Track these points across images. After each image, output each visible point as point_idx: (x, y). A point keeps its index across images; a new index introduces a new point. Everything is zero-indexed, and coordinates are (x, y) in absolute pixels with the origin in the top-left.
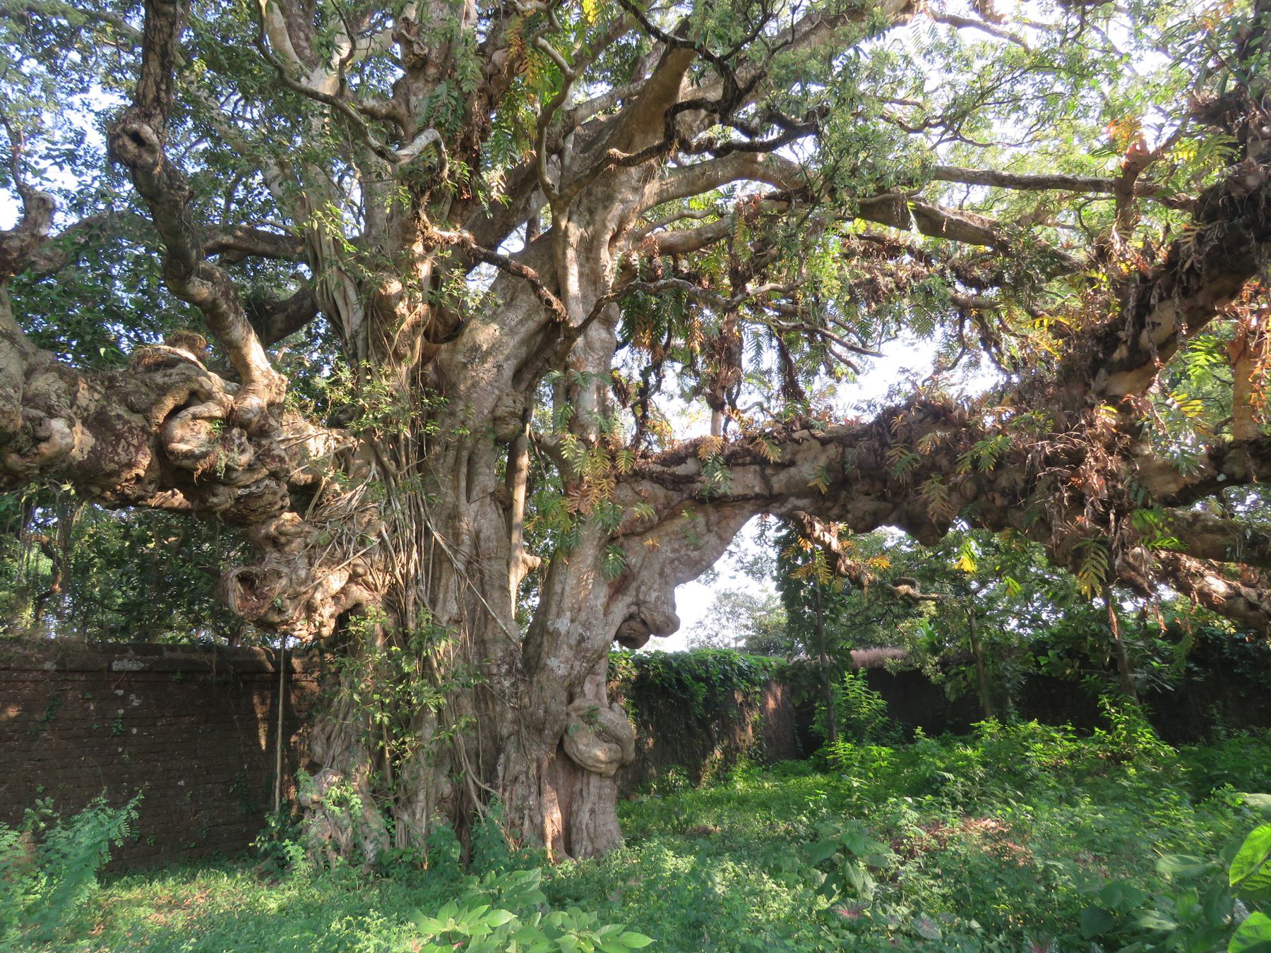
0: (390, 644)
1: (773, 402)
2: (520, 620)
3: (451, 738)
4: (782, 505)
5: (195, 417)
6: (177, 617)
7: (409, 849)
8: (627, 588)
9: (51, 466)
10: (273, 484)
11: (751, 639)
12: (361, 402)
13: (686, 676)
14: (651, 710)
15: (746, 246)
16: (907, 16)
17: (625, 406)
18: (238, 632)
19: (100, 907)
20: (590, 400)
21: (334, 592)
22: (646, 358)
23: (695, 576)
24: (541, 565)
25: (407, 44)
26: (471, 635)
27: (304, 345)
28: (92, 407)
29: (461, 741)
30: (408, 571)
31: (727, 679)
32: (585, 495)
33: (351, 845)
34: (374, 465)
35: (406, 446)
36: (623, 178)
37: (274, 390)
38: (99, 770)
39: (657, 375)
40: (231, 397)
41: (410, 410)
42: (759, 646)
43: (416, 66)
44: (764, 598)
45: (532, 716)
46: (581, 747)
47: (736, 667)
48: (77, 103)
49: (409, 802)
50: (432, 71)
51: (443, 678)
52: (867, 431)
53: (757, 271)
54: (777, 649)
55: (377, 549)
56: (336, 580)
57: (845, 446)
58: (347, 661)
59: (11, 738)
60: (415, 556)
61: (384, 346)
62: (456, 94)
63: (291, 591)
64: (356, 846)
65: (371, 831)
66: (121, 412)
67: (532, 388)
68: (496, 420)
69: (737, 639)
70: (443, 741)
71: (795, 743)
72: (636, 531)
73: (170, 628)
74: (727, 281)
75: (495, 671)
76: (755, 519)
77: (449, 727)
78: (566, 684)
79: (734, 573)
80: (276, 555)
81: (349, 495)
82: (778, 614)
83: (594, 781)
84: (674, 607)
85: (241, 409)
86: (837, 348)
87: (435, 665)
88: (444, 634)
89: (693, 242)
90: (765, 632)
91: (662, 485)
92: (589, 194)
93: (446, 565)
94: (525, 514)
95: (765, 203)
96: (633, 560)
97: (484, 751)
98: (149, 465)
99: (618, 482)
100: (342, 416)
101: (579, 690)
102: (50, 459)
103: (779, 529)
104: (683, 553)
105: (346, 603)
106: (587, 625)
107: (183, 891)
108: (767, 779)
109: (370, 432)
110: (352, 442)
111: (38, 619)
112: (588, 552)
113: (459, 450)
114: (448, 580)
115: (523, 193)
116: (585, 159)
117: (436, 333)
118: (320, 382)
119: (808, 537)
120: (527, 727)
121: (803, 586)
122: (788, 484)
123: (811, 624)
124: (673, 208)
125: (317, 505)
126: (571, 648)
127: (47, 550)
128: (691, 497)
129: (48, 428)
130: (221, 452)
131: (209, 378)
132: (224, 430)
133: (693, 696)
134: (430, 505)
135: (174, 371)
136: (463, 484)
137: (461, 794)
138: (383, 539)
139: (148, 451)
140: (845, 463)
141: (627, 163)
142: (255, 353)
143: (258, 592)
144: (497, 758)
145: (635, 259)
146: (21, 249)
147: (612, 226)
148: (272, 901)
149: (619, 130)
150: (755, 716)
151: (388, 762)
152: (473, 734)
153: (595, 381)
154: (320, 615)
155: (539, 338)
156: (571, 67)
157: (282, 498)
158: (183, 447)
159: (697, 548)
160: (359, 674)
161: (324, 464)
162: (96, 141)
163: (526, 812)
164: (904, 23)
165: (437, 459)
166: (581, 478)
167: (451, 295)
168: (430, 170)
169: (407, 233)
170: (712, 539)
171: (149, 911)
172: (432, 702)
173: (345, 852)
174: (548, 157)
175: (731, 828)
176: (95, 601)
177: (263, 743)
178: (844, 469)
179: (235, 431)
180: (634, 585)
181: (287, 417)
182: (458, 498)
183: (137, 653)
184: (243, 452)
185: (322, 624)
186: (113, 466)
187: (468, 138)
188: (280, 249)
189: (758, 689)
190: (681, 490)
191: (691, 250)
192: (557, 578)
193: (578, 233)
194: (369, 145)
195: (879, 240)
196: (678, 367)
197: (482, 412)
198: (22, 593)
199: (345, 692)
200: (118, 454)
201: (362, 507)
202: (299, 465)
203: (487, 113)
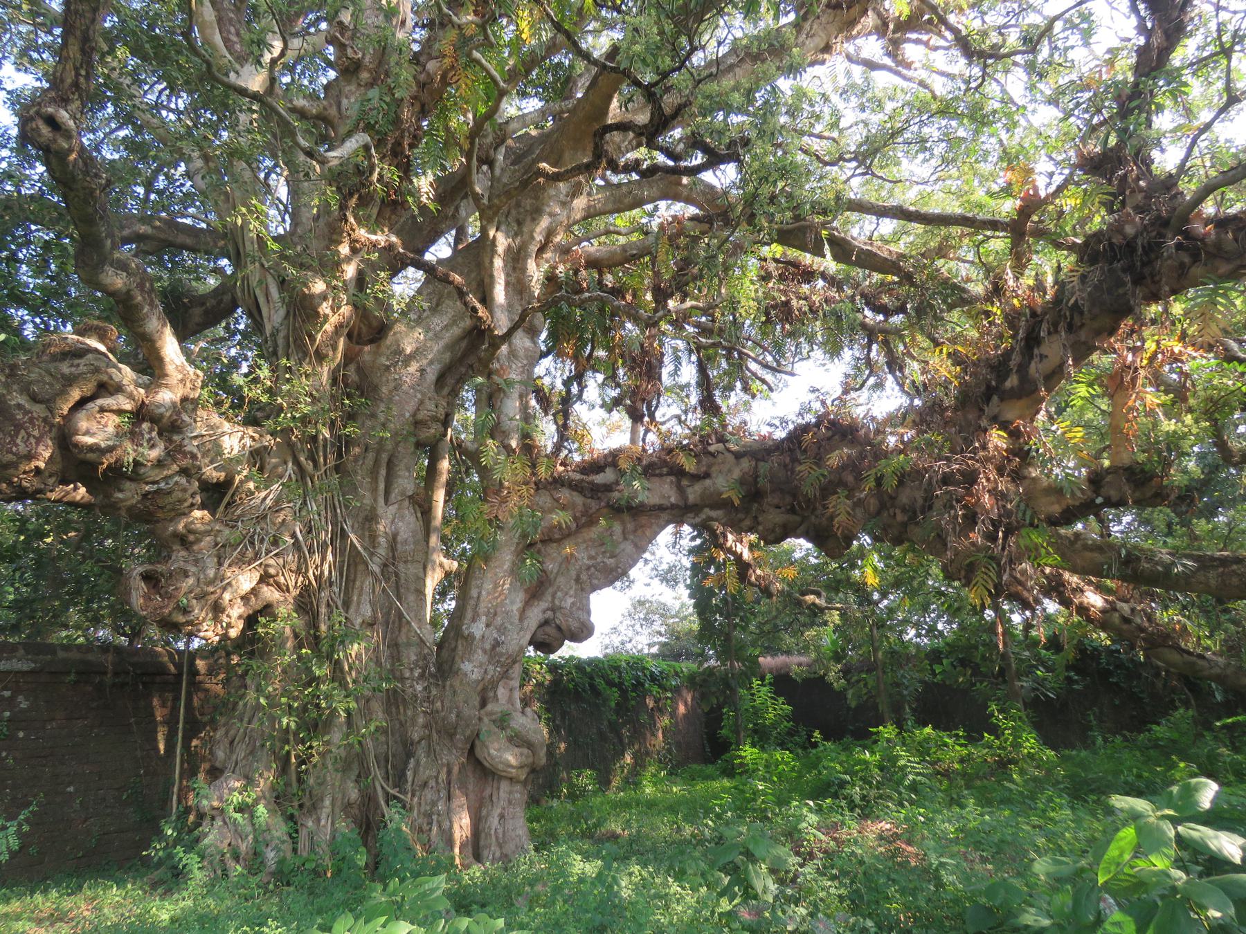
0: (301, 646)
2: (435, 623)
3: (360, 743)
4: (697, 515)
5: (102, 410)
6: (74, 615)
8: (543, 594)
10: (183, 481)
11: (663, 645)
13: (599, 681)
16: (826, 56)
20: (512, 406)
21: (243, 593)
22: (569, 367)
23: (610, 583)
25: (341, 47)
26: (384, 639)
27: (222, 340)
30: (322, 572)
31: (639, 684)
32: (504, 501)
33: (251, 852)
34: (290, 465)
35: (325, 447)
36: (552, 192)
37: (189, 385)
39: (579, 384)
40: (142, 391)
41: (330, 410)
42: (670, 653)
43: (349, 70)
44: (677, 605)
45: (443, 719)
46: (492, 751)
47: (648, 673)
49: (314, 808)
50: (365, 75)
51: (354, 682)
52: (779, 446)
54: (689, 655)
55: (291, 548)
56: (246, 580)
57: (757, 460)
58: (254, 663)
60: (330, 557)
61: (305, 345)
66: (22, 402)
67: (455, 393)
68: (417, 424)
69: (650, 645)
70: (351, 746)
72: (554, 537)
73: (66, 627)
74: (649, 297)
75: (407, 675)
76: (670, 528)
77: (358, 732)
78: (479, 688)
79: (648, 581)
80: (183, 553)
81: (263, 494)
83: (504, 786)
84: (589, 613)
85: (152, 403)
86: (753, 366)
87: (347, 668)
90: (678, 638)
91: (581, 492)
92: (518, 205)
93: (361, 567)
94: (444, 518)
95: (688, 224)
96: (550, 566)
97: (394, 756)
98: (51, 457)
99: (538, 489)
100: (259, 414)
101: (492, 694)
105: (256, 604)
106: (502, 630)
107: (67, 903)
108: (675, 783)
109: (287, 431)
110: (268, 440)
112: (506, 558)
113: (378, 452)
114: (363, 583)
115: (453, 200)
116: (515, 171)
117: (359, 335)
118: (238, 379)
119: (721, 547)
120: (438, 732)
121: (714, 594)
124: (599, 223)
125: (229, 504)
126: (485, 652)
128: (608, 506)
130: (129, 446)
131: (119, 370)
132: (133, 424)
133: (606, 700)
134: (347, 507)
135: (82, 361)
136: (382, 486)
137: (368, 799)
138: (297, 542)
139: (50, 443)
141: (556, 178)
142: (170, 347)
143: (162, 591)
144: (406, 763)
147: (539, 237)
149: (549, 145)
150: (666, 721)
151: (293, 767)
152: (383, 738)
153: (515, 393)
154: (228, 616)
155: (464, 344)
156: (505, 81)
157: (192, 496)
158: (89, 440)
159: (612, 557)
161: (239, 462)
163: (435, 817)
164: (823, 62)
165: (356, 461)
166: (501, 484)
167: (376, 298)
169: (334, 234)
175: (639, 832)
177: (162, 747)
178: (756, 482)
179: (145, 426)
180: (550, 590)
181: (201, 413)
182: (375, 500)
183: (27, 653)
184: (152, 447)
185: (229, 626)
188: (202, 242)
189: (669, 695)
191: (616, 265)
195: (795, 264)
196: (600, 377)
197: (403, 415)
199: (251, 695)
200: (17, 445)
201: (277, 507)
202: (212, 462)
203: (419, 120)
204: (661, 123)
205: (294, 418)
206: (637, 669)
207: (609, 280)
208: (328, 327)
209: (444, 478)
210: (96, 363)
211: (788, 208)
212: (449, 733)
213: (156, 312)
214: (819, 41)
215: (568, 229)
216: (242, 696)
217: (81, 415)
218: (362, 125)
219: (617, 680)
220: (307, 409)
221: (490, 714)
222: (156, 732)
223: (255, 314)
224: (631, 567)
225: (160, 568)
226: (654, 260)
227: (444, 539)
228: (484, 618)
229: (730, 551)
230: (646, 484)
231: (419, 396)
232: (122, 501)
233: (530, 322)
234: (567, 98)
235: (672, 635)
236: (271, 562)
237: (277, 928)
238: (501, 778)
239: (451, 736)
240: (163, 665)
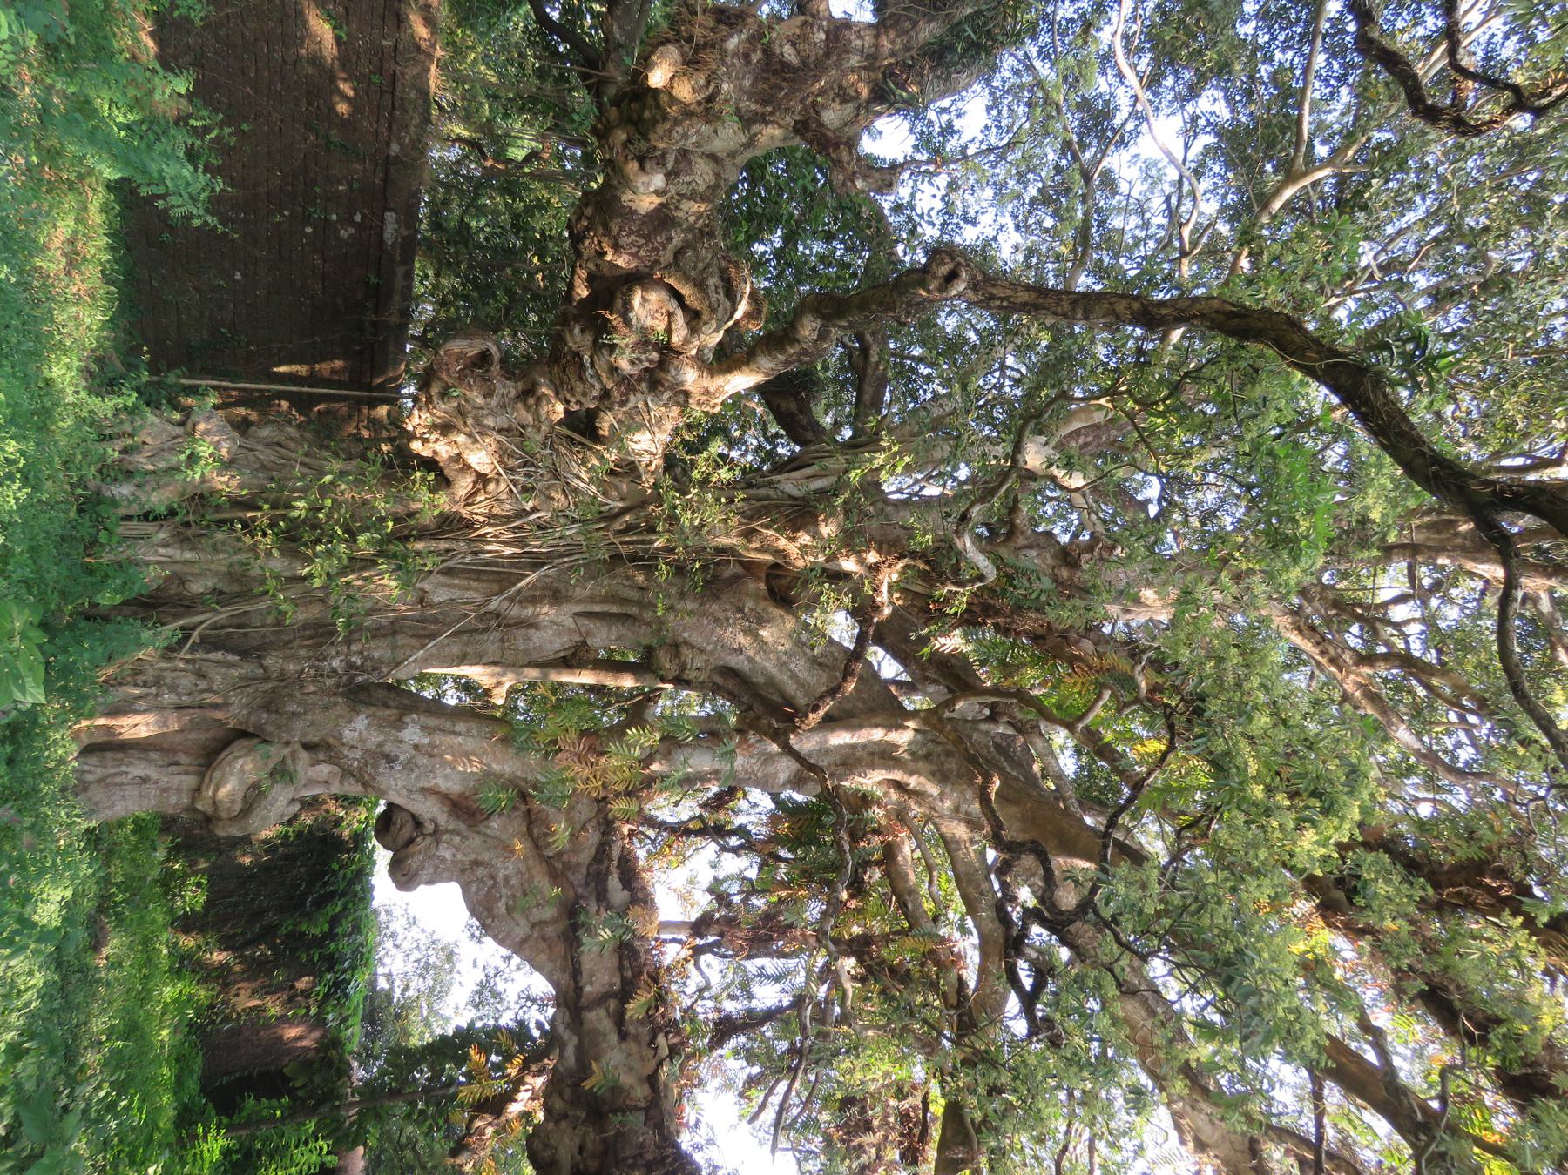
0: (396, 520)
1: (710, 1004)
2: (421, 678)
3: (266, 592)
4: (568, 1026)
5: (670, 315)
6: (450, 282)
7: (115, 539)
8: (458, 817)
9: (614, 170)
10: (595, 393)
11: (389, 996)
12: (694, 491)
14: (291, 858)
15: (901, 954)
16: (1191, 1144)
17: (701, 806)
18: (427, 347)
19: (81, 177)
20: (702, 762)
21: (465, 456)
22: (759, 830)
23: (474, 912)
24: (494, 707)
25: (1090, 548)
26: (404, 618)
27: (765, 430)
28: (680, 214)
29: (262, 606)
30: (489, 543)
32: (580, 758)
33: (131, 468)
34: (620, 504)
35: (643, 542)
36: (969, 795)
37: (703, 398)
38: (263, 190)
39: (741, 847)
40: (694, 352)
41: (686, 547)
42: (378, 1010)
43: (1067, 557)
44: (447, 1011)
45: (290, 696)
46: (241, 762)
47: (347, 976)
48: (1001, 220)
49: (183, 540)
50: (1065, 573)
51: (348, 583)
52: (668, 1139)
53: (869, 969)
54: (371, 1036)
55: (519, 507)
56: (481, 458)
57: (647, 1110)
58: (376, 467)
59: (310, 103)
60: (508, 551)
61: (760, 518)
62: (1043, 598)
63: (469, 408)
64: (129, 474)
65: (149, 494)
66: (675, 241)
67: (717, 690)
68: (675, 647)
69: (389, 976)
70: (263, 582)
71: (229, 1074)
73: (437, 275)
74: (856, 930)
75: (354, 648)
76: (551, 990)
77: (281, 590)
78: (331, 740)
79: (480, 965)
80: (513, 393)
81: (584, 476)
82: (423, 1033)
83: (190, 781)
84: (430, 882)
86: (782, 1086)
87: (366, 574)
88: (406, 584)
89: (900, 886)
90: (398, 1016)
92: (948, 754)
93: (495, 587)
94: (561, 684)
95: (953, 976)
96: (495, 824)
97: (245, 635)
99: (598, 801)
100: (678, 470)
101: (321, 757)
102: (621, 171)
103: (539, 1025)
104: (504, 891)
106: (409, 766)
107: (92, 271)
108: (175, 1031)
109: (659, 500)
111: (454, 141)
112: (507, 765)
113: (639, 603)
114: (476, 590)
115: (944, 676)
117: (778, 577)
118: (717, 447)
119: (525, 1068)
120: (273, 690)
121: (459, 1066)
122: (595, 1032)
123: (405, 1083)
124: (938, 856)
125: (572, 440)
126: (380, 745)
127: (533, 155)
128: (578, 897)
129: (653, 172)
130: (631, 340)
131: (716, 331)
133: (308, 916)
134: (570, 568)
135: (722, 296)
136: (597, 608)
137: (188, 605)
138: (528, 513)
140: (624, 1113)
141: (984, 799)
142: (742, 381)
144: (233, 651)
145: (877, 812)
146: (840, 161)
147: (913, 782)
148: (63, 372)
149: (1023, 788)
150: (274, 1009)
151: (240, 514)
152: (270, 620)
153: (724, 767)
154: (437, 440)
155: (775, 697)
157: (578, 402)
158: (637, 300)
159: (509, 910)
160: (358, 483)
162: (968, 236)
163: (154, 690)
164: (1183, 1142)
165: (627, 578)
166: (602, 753)
167: (821, 594)
168: (956, 570)
169: (893, 546)
170: (521, 931)
171: (68, 233)
172: (316, 570)
173: (121, 461)
174: (985, 705)
175: (99, 981)
176: (475, 199)
177: (283, 369)
178: (615, 1112)
179: (655, 356)
180: (462, 827)
181: (675, 411)
182: (580, 601)
183: (404, 238)
184: (632, 363)
185: (425, 441)
186: (615, 229)
187: (997, 613)
189: (313, 1010)
190: (587, 884)
191: (891, 883)
192: (474, 725)
193: (900, 742)
194: (972, 504)
195: (924, 1136)
196: (752, 873)
197: (685, 630)
198: (488, 128)
199: (337, 465)
200: (628, 235)
202: (619, 421)
203: (1027, 634)
204: (1058, 924)
205: (675, 507)
206: (354, 959)
207: (873, 875)
208: (782, 543)
209: (610, 681)
210: (721, 309)
211: (986, 1116)
212: (271, 704)
213: (780, 367)
214: (1208, 1134)
215: (928, 819)
216: (336, 455)
217: (664, 295)
218: (1010, 571)
219: (339, 930)
220: (685, 520)
221: (294, 755)
222: (301, 363)
223: (793, 464)
224: (495, 937)
225: (496, 369)
226: (903, 933)
227: (532, 685)
228: (426, 741)
229: (518, 1082)
230: (609, 947)
231: (710, 648)
232: (571, 331)
233: (810, 778)
234: (1081, 804)
235: (403, 1007)
236: (503, 486)
237: (17, 499)
238: (202, 775)
239: (266, 707)
240: (383, 372)
